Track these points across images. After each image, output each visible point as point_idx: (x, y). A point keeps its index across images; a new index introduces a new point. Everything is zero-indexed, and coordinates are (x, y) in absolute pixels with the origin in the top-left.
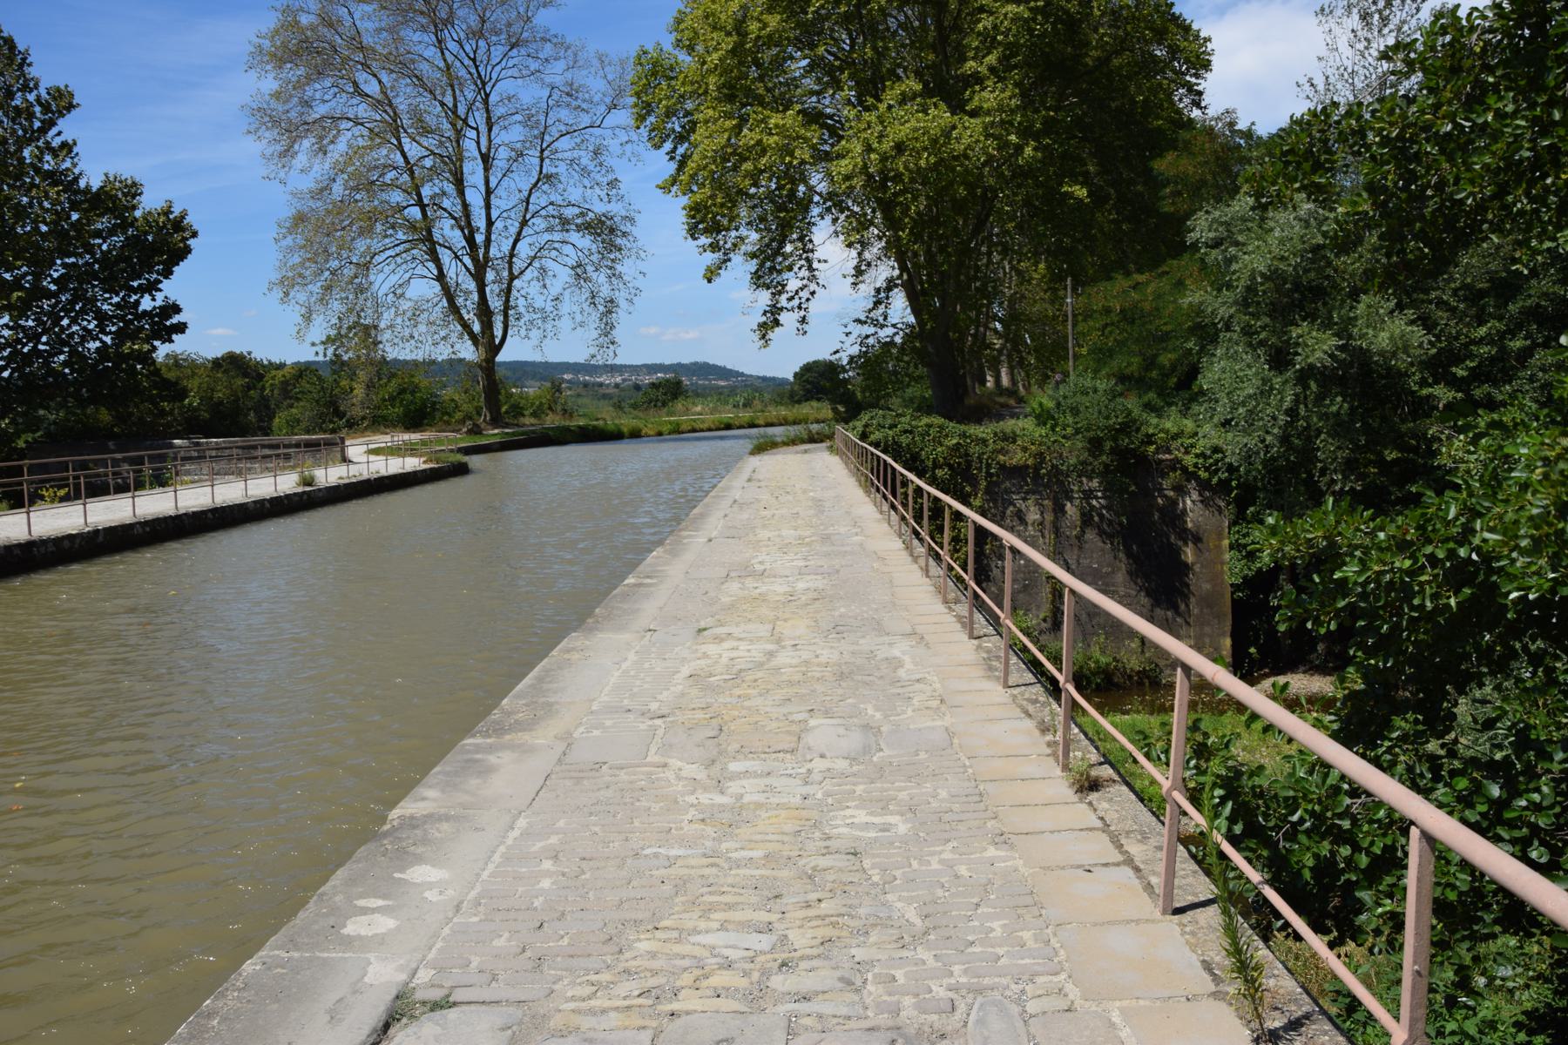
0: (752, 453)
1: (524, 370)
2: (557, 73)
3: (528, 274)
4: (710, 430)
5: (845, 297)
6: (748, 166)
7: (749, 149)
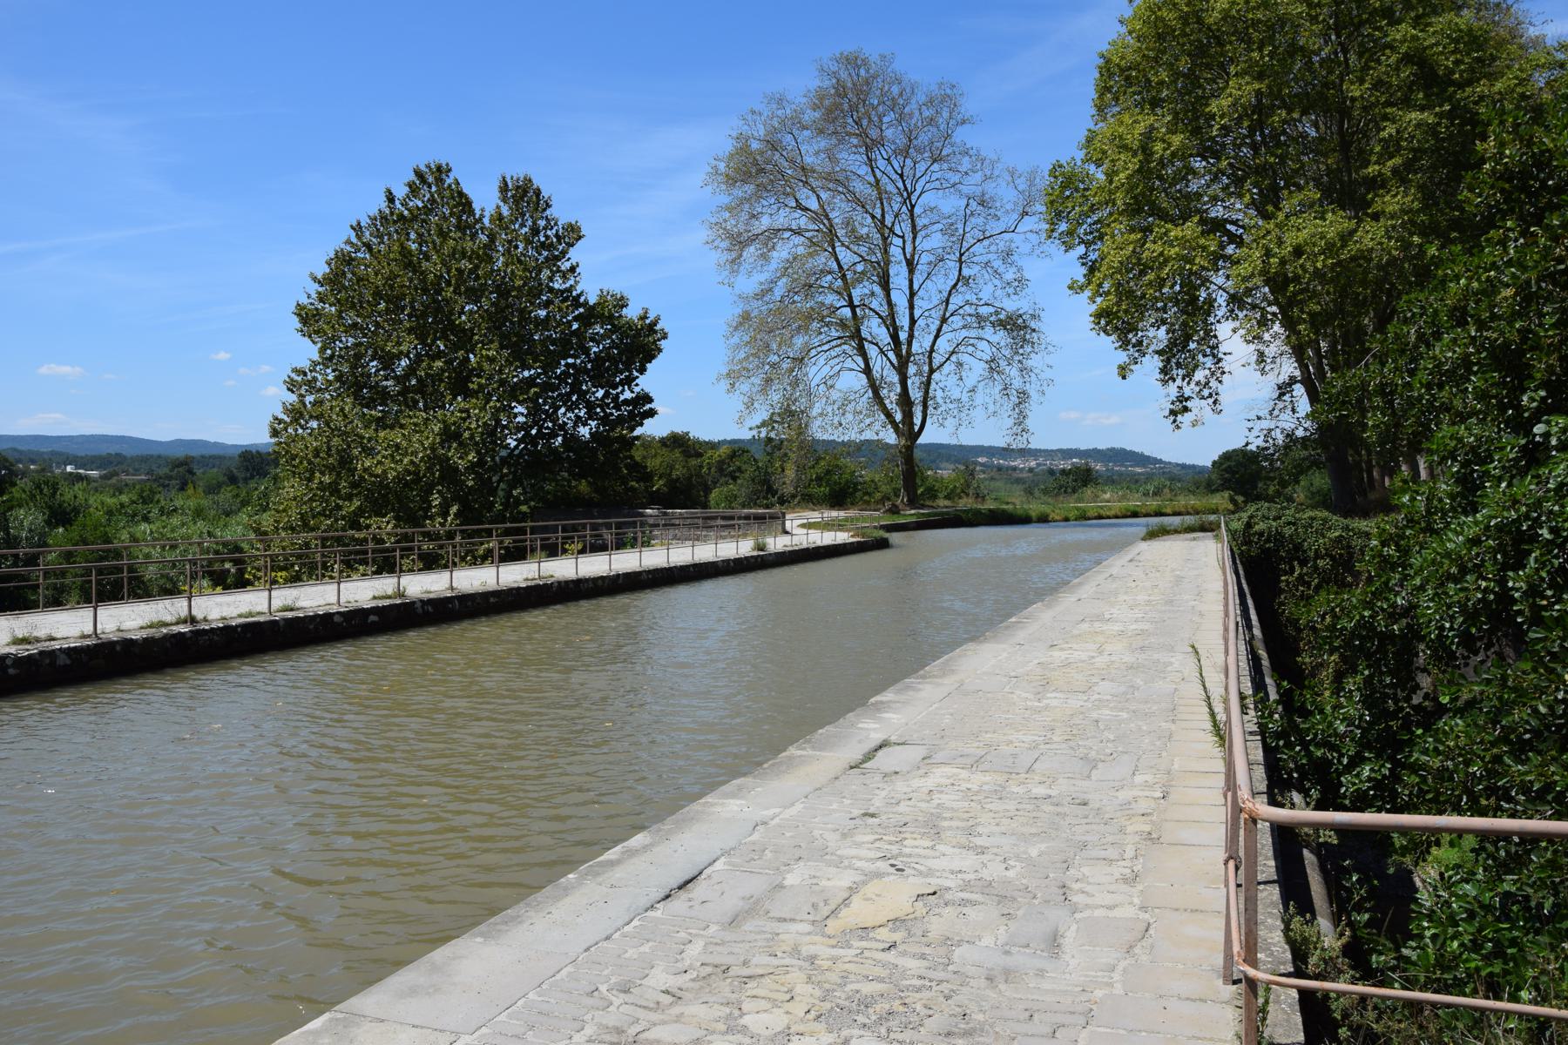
0: (1144, 539)
1: (941, 452)
2: (972, 184)
3: (948, 367)
4: (1117, 517)
5: (1251, 393)
6: (1151, 276)
7: (1154, 260)
